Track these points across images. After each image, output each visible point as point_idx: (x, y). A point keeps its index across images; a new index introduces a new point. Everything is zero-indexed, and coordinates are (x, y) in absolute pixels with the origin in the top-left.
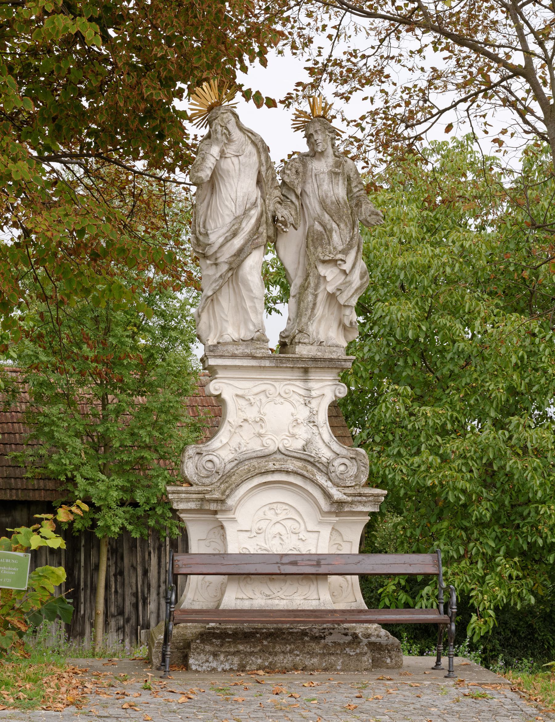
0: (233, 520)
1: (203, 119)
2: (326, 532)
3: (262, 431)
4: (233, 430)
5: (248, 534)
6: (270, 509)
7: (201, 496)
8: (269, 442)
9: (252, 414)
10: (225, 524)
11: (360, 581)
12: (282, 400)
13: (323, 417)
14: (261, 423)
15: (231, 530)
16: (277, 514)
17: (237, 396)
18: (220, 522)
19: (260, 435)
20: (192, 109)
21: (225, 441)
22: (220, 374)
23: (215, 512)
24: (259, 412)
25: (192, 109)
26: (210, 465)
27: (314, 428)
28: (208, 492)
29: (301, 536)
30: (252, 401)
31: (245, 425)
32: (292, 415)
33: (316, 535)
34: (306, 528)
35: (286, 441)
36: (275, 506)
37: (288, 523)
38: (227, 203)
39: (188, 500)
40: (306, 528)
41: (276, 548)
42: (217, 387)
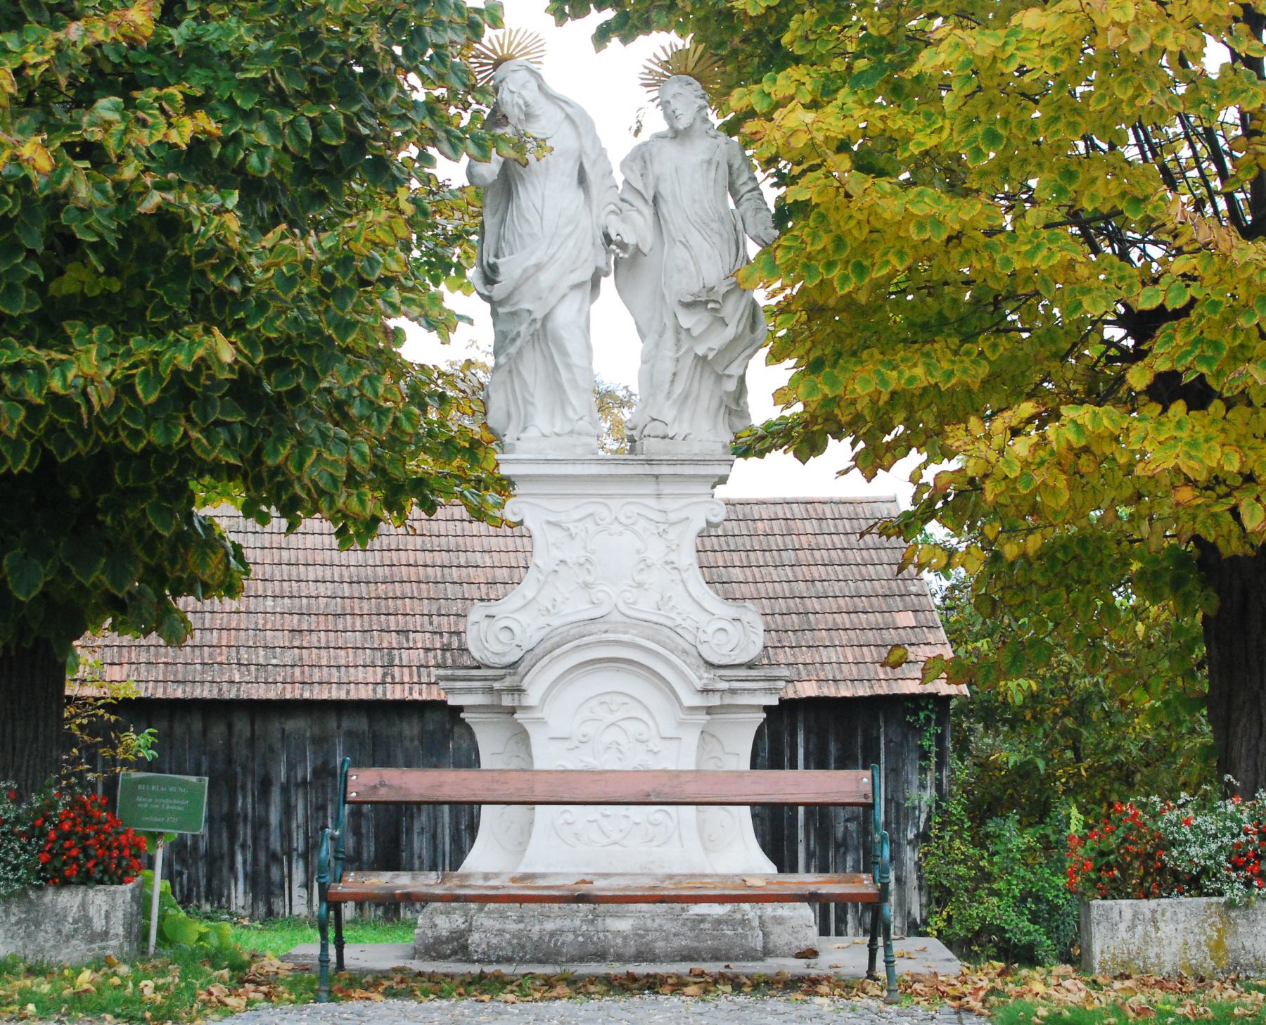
0: (541, 722)
1: (519, 44)
2: (691, 738)
3: (590, 579)
4: (541, 578)
5: (567, 744)
6: (602, 703)
7: (488, 684)
8: (600, 595)
9: (573, 554)
10: (529, 728)
11: (754, 816)
12: (621, 529)
13: (687, 557)
14: (588, 565)
15: (538, 738)
16: (611, 711)
17: (549, 522)
18: (521, 725)
19: (587, 586)
20: (490, 41)
21: (530, 595)
22: (519, 489)
23: (512, 711)
24: (585, 548)
25: (490, 41)
26: (505, 636)
27: (675, 572)
28: (447, 679)
29: (651, 746)
30: (573, 531)
31: (561, 568)
32: (638, 552)
33: (675, 744)
34: (659, 732)
35: (628, 595)
36: (606, 698)
37: (631, 727)
38: (528, 216)
39: (470, 691)
40: (659, 732)
41: (609, 762)
42: (516, 510)
